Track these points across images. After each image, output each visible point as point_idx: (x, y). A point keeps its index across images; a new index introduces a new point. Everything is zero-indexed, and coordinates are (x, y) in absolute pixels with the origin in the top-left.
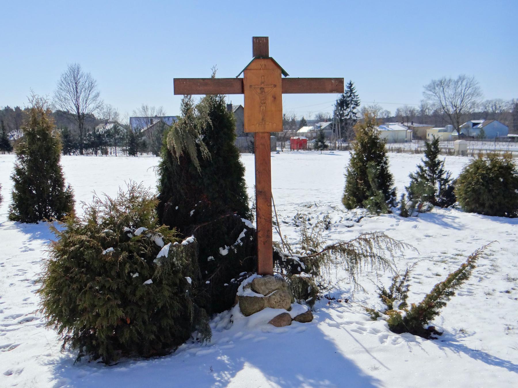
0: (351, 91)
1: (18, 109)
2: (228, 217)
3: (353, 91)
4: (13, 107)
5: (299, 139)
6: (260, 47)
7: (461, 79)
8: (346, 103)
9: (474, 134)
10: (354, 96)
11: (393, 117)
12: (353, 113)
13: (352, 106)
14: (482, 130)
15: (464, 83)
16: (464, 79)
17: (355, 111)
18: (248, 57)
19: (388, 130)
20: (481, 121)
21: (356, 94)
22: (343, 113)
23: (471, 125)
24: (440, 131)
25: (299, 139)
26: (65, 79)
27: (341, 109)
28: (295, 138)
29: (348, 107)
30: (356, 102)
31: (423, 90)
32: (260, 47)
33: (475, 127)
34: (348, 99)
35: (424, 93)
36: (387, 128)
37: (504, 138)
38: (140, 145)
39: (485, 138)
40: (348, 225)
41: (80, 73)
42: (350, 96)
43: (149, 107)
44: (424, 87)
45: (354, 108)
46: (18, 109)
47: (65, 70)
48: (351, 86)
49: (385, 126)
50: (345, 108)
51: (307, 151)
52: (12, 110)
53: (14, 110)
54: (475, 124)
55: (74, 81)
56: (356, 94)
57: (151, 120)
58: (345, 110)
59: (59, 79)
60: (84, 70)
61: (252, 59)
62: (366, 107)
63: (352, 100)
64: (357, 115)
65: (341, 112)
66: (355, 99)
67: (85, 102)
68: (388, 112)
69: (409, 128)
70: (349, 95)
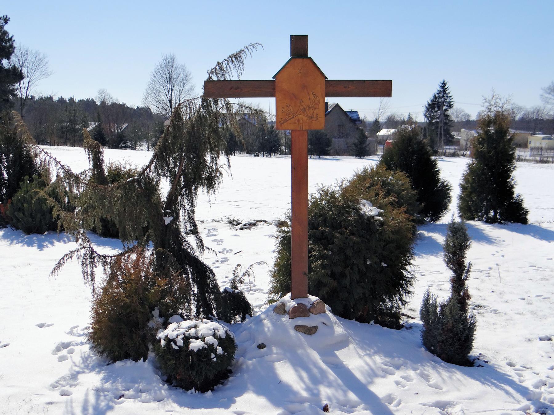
1: (71, 100)
3: (447, 92)
4: (66, 98)
6: (299, 45)
10: (447, 97)
11: (473, 121)
21: (449, 95)
24: (544, 138)
26: (159, 70)
30: (449, 103)
31: (541, 92)
32: (299, 45)
34: (440, 100)
35: (542, 95)
42: (443, 97)
44: (543, 89)
46: (71, 100)
47: (157, 60)
48: (444, 86)
50: (436, 109)
51: (283, 156)
53: (67, 101)
59: (153, 70)
60: (179, 62)
61: (288, 57)
65: (432, 114)
66: (448, 100)
68: (468, 116)
70: (441, 95)
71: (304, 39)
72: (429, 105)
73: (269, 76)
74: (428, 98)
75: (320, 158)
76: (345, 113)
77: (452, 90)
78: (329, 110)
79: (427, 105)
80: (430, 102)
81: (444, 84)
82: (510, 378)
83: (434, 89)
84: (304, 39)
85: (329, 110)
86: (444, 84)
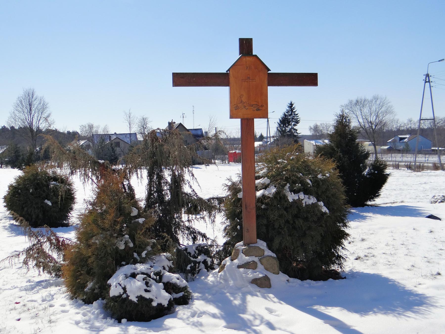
0: (292, 110)
1: (12, 128)
5: (235, 152)
6: (246, 46)
7: (376, 99)
8: (287, 120)
9: (401, 147)
12: (294, 129)
13: (293, 124)
14: (407, 144)
15: (378, 102)
16: (378, 99)
17: (295, 127)
20: (408, 136)
21: (296, 113)
22: (286, 130)
23: (398, 140)
25: (235, 152)
27: (283, 126)
28: (232, 152)
29: (289, 125)
32: (246, 46)
33: (401, 141)
37: (428, 151)
39: (410, 151)
40: (371, 249)
41: (35, 97)
42: (292, 114)
43: (94, 126)
45: (294, 125)
47: (21, 93)
49: (321, 141)
52: (7, 129)
54: (401, 139)
55: (29, 102)
57: (110, 137)
58: (287, 127)
60: (38, 94)
62: (319, 124)
63: (293, 119)
64: (297, 132)
65: (284, 129)
67: (38, 122)
72: (280, 121)
77: (298, 109)
79: (279, 122)
80: (281, 119)
81: (291, 105)
86: (291, 105)
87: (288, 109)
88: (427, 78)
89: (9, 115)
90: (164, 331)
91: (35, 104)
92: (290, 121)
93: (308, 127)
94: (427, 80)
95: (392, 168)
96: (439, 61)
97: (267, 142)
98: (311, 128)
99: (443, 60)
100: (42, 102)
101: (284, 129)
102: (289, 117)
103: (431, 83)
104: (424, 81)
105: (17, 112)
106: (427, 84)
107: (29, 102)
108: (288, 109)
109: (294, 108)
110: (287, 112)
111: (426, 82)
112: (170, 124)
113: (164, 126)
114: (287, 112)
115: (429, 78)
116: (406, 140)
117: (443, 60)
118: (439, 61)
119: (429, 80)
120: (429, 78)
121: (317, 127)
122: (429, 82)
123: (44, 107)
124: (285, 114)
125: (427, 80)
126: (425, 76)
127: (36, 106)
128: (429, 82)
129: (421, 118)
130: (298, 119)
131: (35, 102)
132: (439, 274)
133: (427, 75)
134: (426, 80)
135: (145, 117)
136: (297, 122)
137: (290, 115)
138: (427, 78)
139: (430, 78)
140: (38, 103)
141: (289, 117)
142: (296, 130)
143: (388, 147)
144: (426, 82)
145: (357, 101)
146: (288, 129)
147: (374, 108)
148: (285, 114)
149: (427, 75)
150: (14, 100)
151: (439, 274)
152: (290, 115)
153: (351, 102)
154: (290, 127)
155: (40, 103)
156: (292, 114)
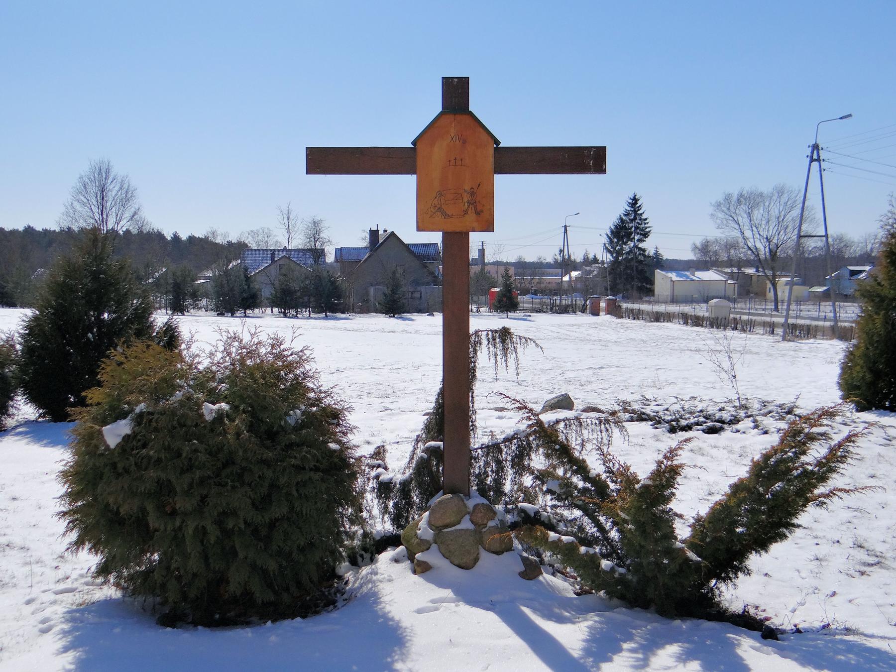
0: (635, 212)
2: (526, 551)
6: (456, 92)
12: (640, 249)
13: (637, 237)
15: (785, 198)
16: (783, 193)
17: (641, 245)
18: (434, 106)
19: (693, 280)
20: (867, 268)
21: (644, 217)
22: (622, 249)
27: (618, 242)
32: (456, 92)
36: (692, 277)
38: (794, 267)
45: (640, 240)
47: (84, 168)
49: (688, 273)
54: (854, 273)
55: (100, 186)
56: (644, 217)
57: (273, 254)
58: (625, 244)
60: (118, 170)
61: (439, 109)
65: (618, 248)
69: (731, 276)
71: (464, 83)
72: (612, 232)
73: (474, 106)
74: (610, 221)
75: (326, 318)
76: (407, 246)
77: (648, 210)
78: (381, 241)
79: (609, 234)
81: (635, 201)
82: (45, 442)
83: (621, 208)
84: (464, 83)
85: (381, 241)
86: (635, 201)
87: (629, 209)
88: (815, 152)
89: (63, 209)
90: (708, 625)
91: (113, 190)
92: (631, 233)
93: (689, 247)
94: (815, 157)
95: (761, 332)
96: (841, 118)
97: (590, 272)
98: (695, 248)
99: (850, 115)
100: (126, 186)
101: (618, 248)
102: (631, 225)
103: (822, 163)
104: (809, 159)
105: (77, 206)
106: (815, 165)
107: (100, 186)
108: (629, 209)
109: (640, 208)
110: (625, 215)
111: (812, 161)
112: (374, 234)
113: (358, 240)
114: (625, 215)
115: (818, 153)
116: (864, 275)
117: (850, 115)
118: (841, 118)
119: (819, 156)
120: (818, 153)
121: (707, 246)
122: (818, 160)
123: (127, 198)
124: (621, 219)
125: (815, 157)
126: (810, 149)
127: (114, 193)
128: (818, 160)
129: (802, 234)
130: (648, 230)
131: (111, 187)
132: (838, 542)
133: (816, 147)
134: (812, 157)
135: (317, 218)
136: (646, 235)
137: (632, 221)
138: (815, 152)
139: (821, 152)
140: (117, 188)
141: (631, 225)
142: (644, 250)
143: (825, 288)
144: (812, 161)
145: (741, 195)
146: (626, 248)
147: (775, 212)
148: (621, 219)
149: (816, 147)
150: (73, 182)
151: (838, 542)
152: (632, 221)
153: (728, 198)
154: (632, 244)
155: (121, 188)
156: (635, 219)
